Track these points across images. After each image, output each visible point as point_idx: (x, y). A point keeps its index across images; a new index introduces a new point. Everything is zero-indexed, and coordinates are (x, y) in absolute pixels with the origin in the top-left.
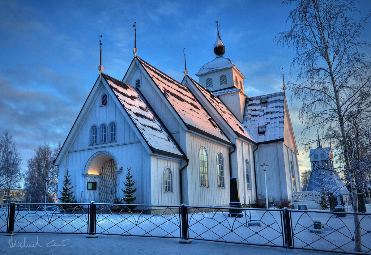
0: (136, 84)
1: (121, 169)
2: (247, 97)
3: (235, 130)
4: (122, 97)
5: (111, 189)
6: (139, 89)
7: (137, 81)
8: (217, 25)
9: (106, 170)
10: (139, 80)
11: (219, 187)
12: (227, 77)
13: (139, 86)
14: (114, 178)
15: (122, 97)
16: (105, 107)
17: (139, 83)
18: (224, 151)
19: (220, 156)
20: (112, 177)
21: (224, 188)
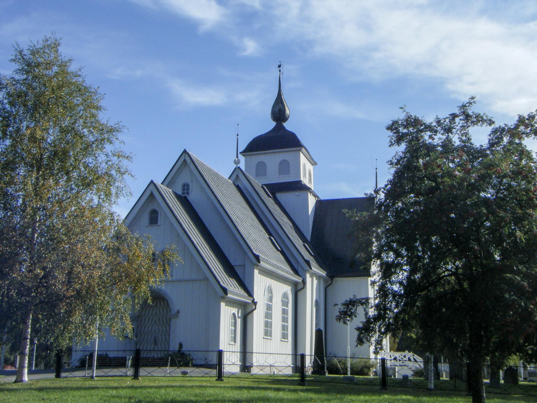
0: (183, 189)
1: (178, 312)
2: (318, 197)
3: (255, 252)
4: (273, 205)
5: (155, 337)
6: (188, 197)
7: (184, 186)
8: (280, 71)
9: (147, 311)
10: (188, 185)
11: (283, 340)
12: (290, 164)
13: (188, 193)
14: (160, 322)
15: (273, 205)
16: (154, 228)
17: (188, 189)
18: (288, 289)
19: (285, 295)
20: (158, 322)
21: (270, 338)
